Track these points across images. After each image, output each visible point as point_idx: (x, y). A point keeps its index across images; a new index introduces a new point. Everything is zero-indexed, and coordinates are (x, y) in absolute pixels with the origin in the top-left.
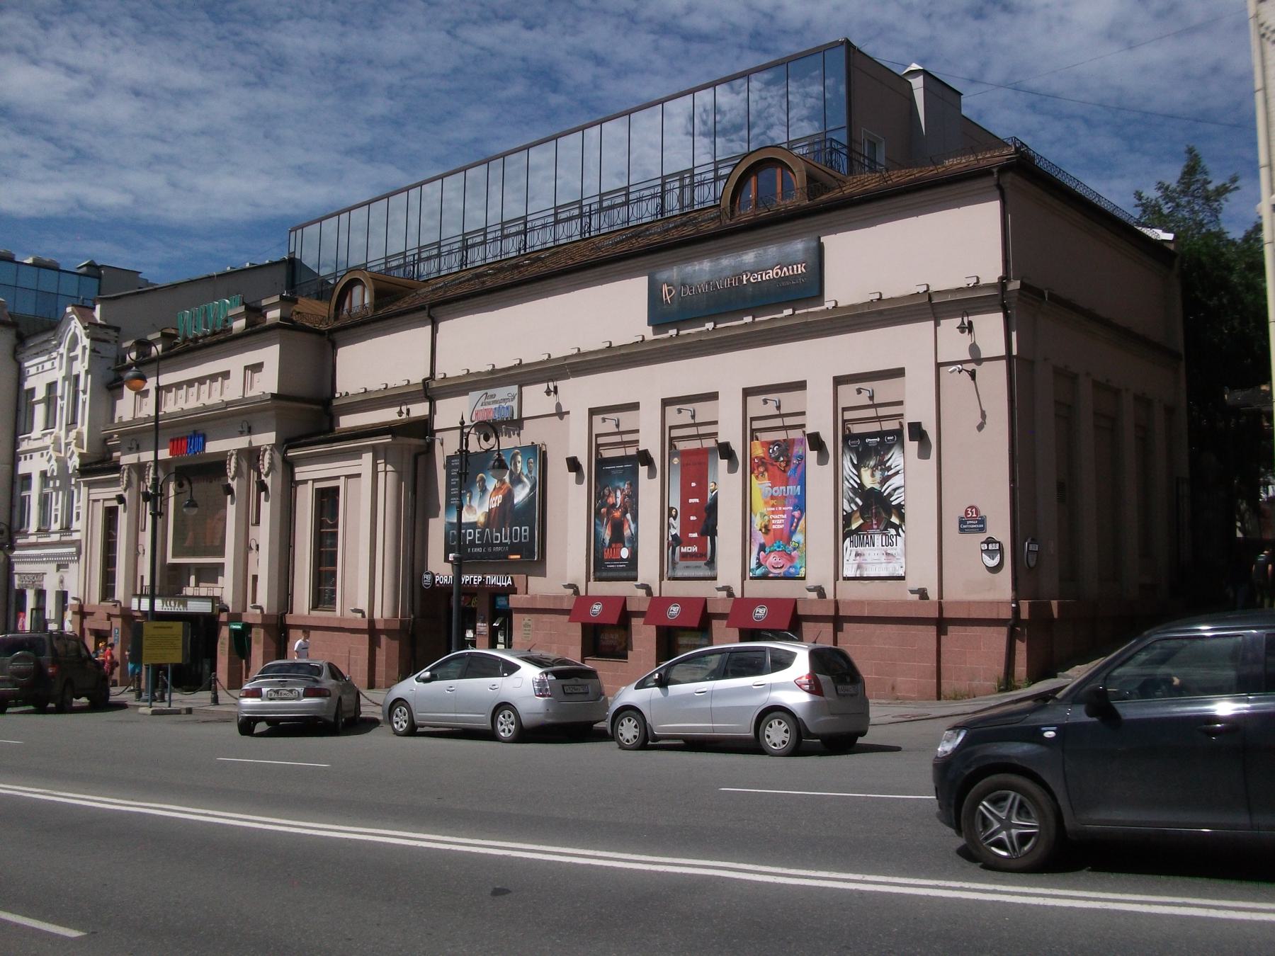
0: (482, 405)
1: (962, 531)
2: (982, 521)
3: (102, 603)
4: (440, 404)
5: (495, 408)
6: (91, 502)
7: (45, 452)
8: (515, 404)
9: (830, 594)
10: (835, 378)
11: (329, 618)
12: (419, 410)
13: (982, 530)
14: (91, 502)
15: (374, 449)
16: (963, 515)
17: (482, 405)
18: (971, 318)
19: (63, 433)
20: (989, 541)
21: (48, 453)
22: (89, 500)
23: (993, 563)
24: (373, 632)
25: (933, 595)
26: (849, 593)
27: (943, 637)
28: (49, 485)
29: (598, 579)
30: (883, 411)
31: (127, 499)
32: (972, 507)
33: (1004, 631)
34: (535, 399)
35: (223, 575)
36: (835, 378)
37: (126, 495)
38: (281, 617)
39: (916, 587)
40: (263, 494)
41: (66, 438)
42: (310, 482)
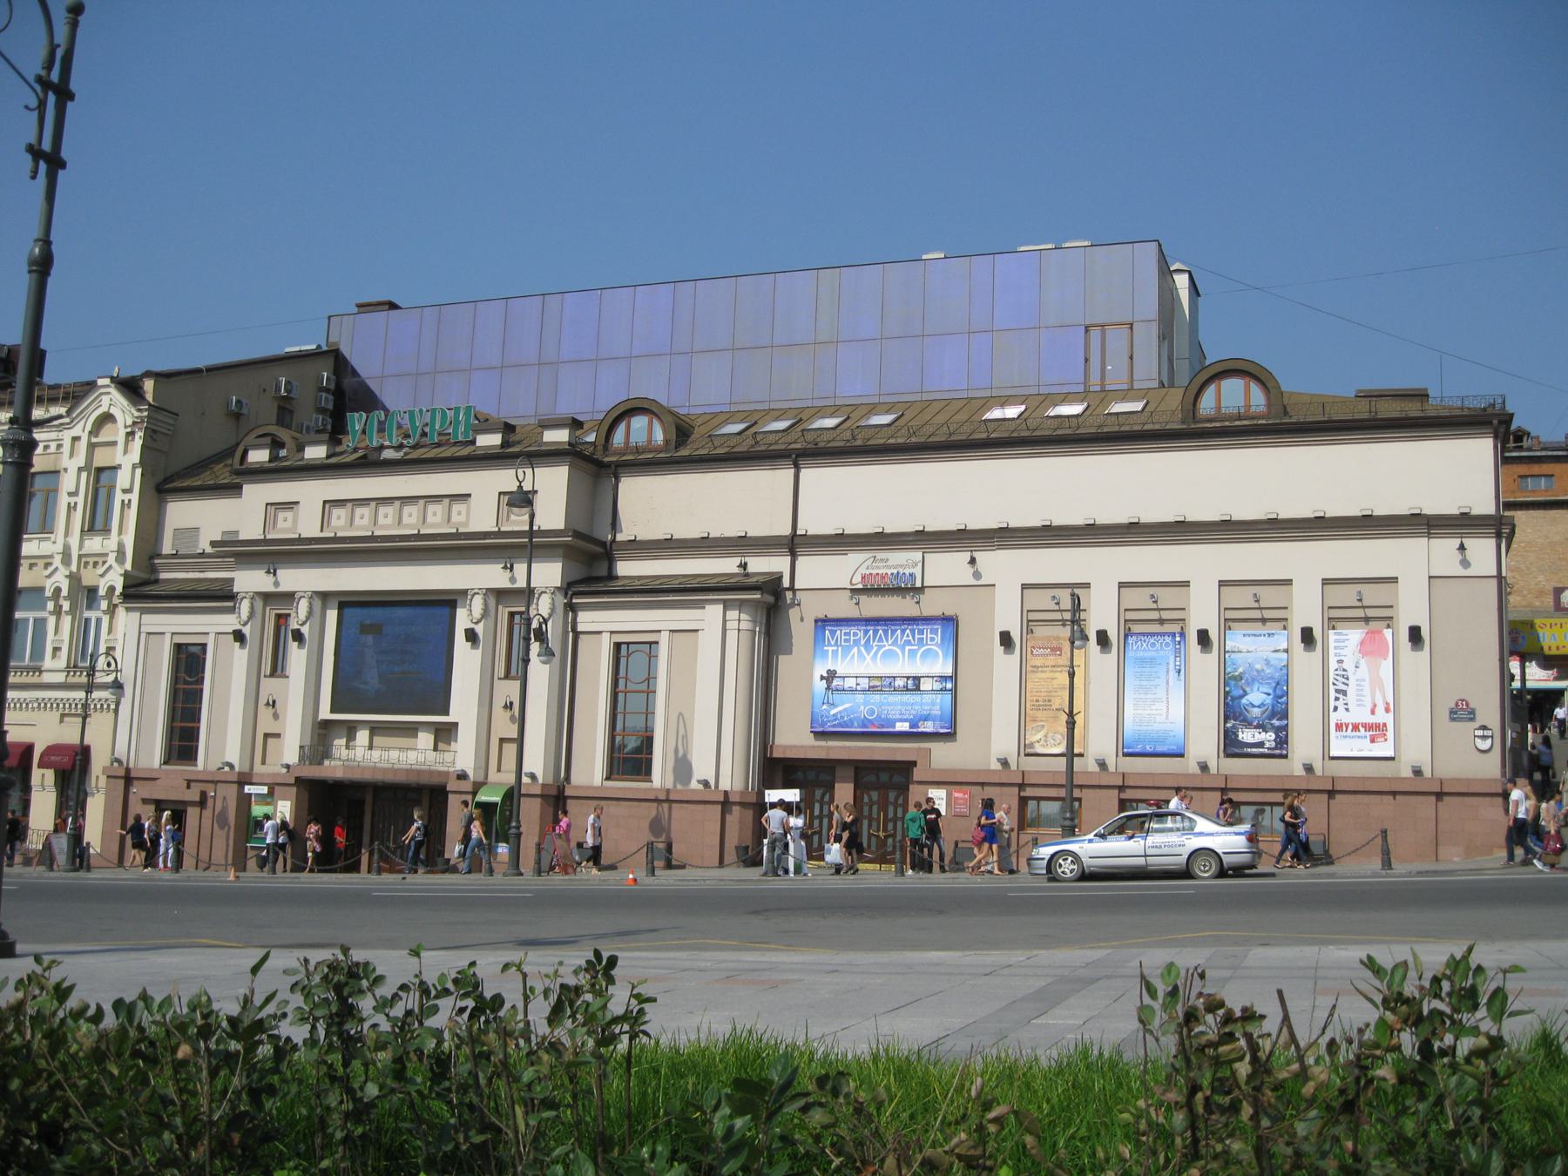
0: (868, 568)
1: (1453, 719)
2: (1473, 712)
3: (164, 767)
4: (802, 562)
5: (892, 574)
6: (143, 636)
7: (100, 560)
8: (918, 571)
9: (1013, 766)
10: (1220, 581)
11: (646, 790)
12: (776, 564)
13: (1472, 720)
14: (143, 636)
15: (725, 602)
16: (1453, 706)
17: (868, 568)
18: (747, 559)
19: (74, 541)
20: (1484, 728)
21: (104, 563)
22: (140, 633)
23: (1485, 745)
24: (726, 804)
25: (712, 783)
26: (1031, 764)
27: (727, 816)
28: (46, 606)
29: (1228, 755)
30: (1165, 615)
31: (307, 636)
32: (1463, 700)
33: (719, 807)
34: (946, 567)
35: (456, 741)
36: (1220, 581)
37: (246, 630)
38: (561, 790)
39: (702, 778)
40: (535, 647)
41: (81, 547)
42: (606, 636)
